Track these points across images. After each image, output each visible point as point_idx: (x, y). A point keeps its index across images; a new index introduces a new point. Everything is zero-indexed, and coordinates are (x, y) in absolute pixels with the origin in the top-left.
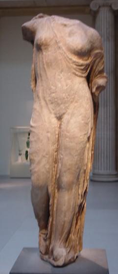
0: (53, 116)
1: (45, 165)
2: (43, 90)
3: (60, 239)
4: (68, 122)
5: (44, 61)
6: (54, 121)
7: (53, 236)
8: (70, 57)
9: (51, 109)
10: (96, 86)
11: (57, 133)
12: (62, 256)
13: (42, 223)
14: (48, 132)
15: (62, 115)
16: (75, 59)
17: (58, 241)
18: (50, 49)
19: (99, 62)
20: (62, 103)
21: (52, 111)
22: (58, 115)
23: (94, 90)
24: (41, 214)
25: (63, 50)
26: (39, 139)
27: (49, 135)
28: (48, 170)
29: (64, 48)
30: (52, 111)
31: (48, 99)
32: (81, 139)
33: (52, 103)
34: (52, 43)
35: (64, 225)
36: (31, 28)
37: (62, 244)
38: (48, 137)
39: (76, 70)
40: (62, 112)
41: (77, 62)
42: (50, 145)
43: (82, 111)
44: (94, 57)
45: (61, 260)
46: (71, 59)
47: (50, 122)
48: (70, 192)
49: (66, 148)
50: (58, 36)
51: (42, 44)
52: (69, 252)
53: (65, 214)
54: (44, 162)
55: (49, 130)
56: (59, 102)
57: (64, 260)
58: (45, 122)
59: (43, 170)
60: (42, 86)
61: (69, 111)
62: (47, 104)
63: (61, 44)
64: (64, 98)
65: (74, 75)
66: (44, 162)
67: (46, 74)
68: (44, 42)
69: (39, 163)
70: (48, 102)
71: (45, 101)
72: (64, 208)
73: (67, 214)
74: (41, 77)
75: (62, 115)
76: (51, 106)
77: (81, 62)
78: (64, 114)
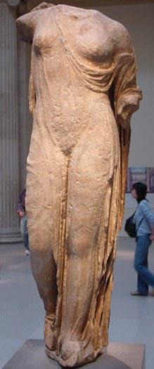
0: (58, 149)
1: (46, 221)
2: (44, 112)
3: (72, 328)
4: (79, 158)
5: (45, 70)
6: (60, 156)
7: (63, 324)
8: (81, 64)
9: (54, 139)
10: (124, 104)
11: (64, 173)
12: (74, 352)
13: (50, 304)
14: (50, 173)
15: (70, 148)
16: (89, 65)
17: (70, 330)
18: (52, 53)
19: (126, 70)
20: (69, 131)
21: (56, 142)
22: (65, 148)
23: (120, 111)
24: (46, 290)
25: (71, 54)
26: (38, 182)
27: (52, 176)
28: (52, 227)
29: (72, 51)
30: (56, 142)
31: (49, 125)
32: (99, 182)
33: (56, 131)
34: (56, 44)
35: (76, 307)
36: (27, 23)
37: (75, 334)
38: (51, 180)
39: (90, 83)
40: (70, 143)
41: (92, 71)
42: (54, 192)
43: (100, 141)
44: (119, 63)
45: (72, 357)
46: (82, 66)
47: (54, 159)
48: (84, 259)
49: (77, 196)
50: (64, 34)
51: (42, 46)
52: (85, 348)
53: (78, 291)
54: (45, 216)
55: (53, 169)
56: (66, 128)
57: (76, 359)
58: (47, 158)
59: (45, 227)
60: (43, 105)
61: (81, 142)
62: (49, 132)
63: (68, 46)
64: (72, 123)
65: (87, 90)
66: (45, 216)
67: (47, 88)
68: (44, 43)
69: (39, 216)
70: (50, 129)
71: (47, 127)
72: (77, 283)
73: (81, 291)
74: (41, 93)
75: (70, 148)
76: (54, 135)
77: (98, 70)
78: (73, 146)
